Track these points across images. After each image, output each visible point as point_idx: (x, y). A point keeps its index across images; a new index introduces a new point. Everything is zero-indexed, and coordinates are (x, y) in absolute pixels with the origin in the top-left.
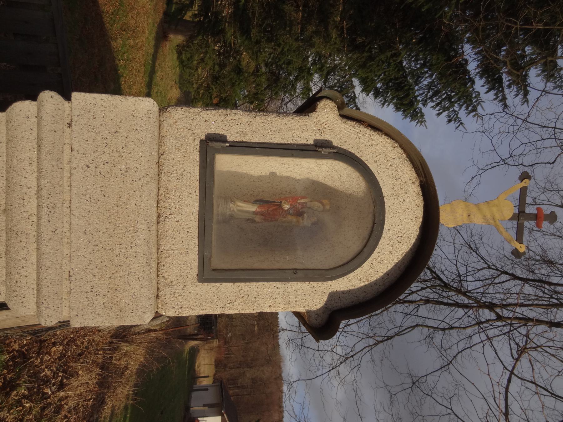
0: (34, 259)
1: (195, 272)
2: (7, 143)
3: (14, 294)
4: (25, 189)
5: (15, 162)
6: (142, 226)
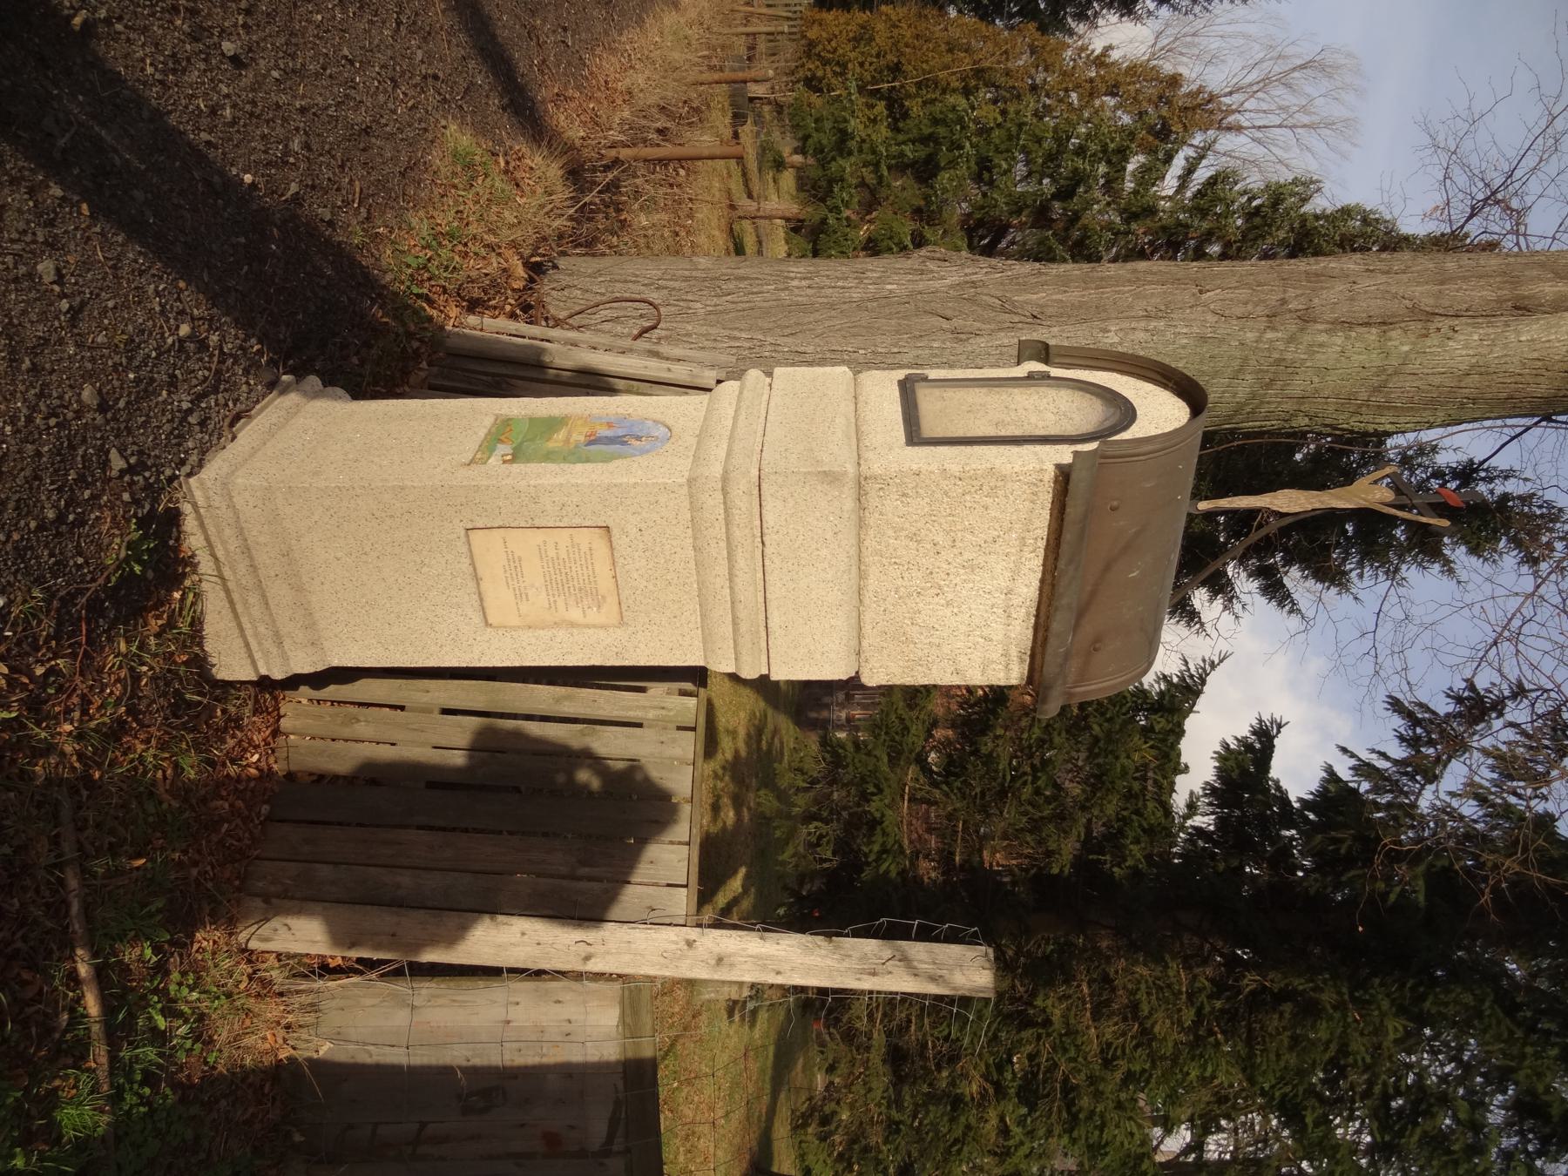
0: (725, 446)
1: (903, 439)
6: (840, 421)
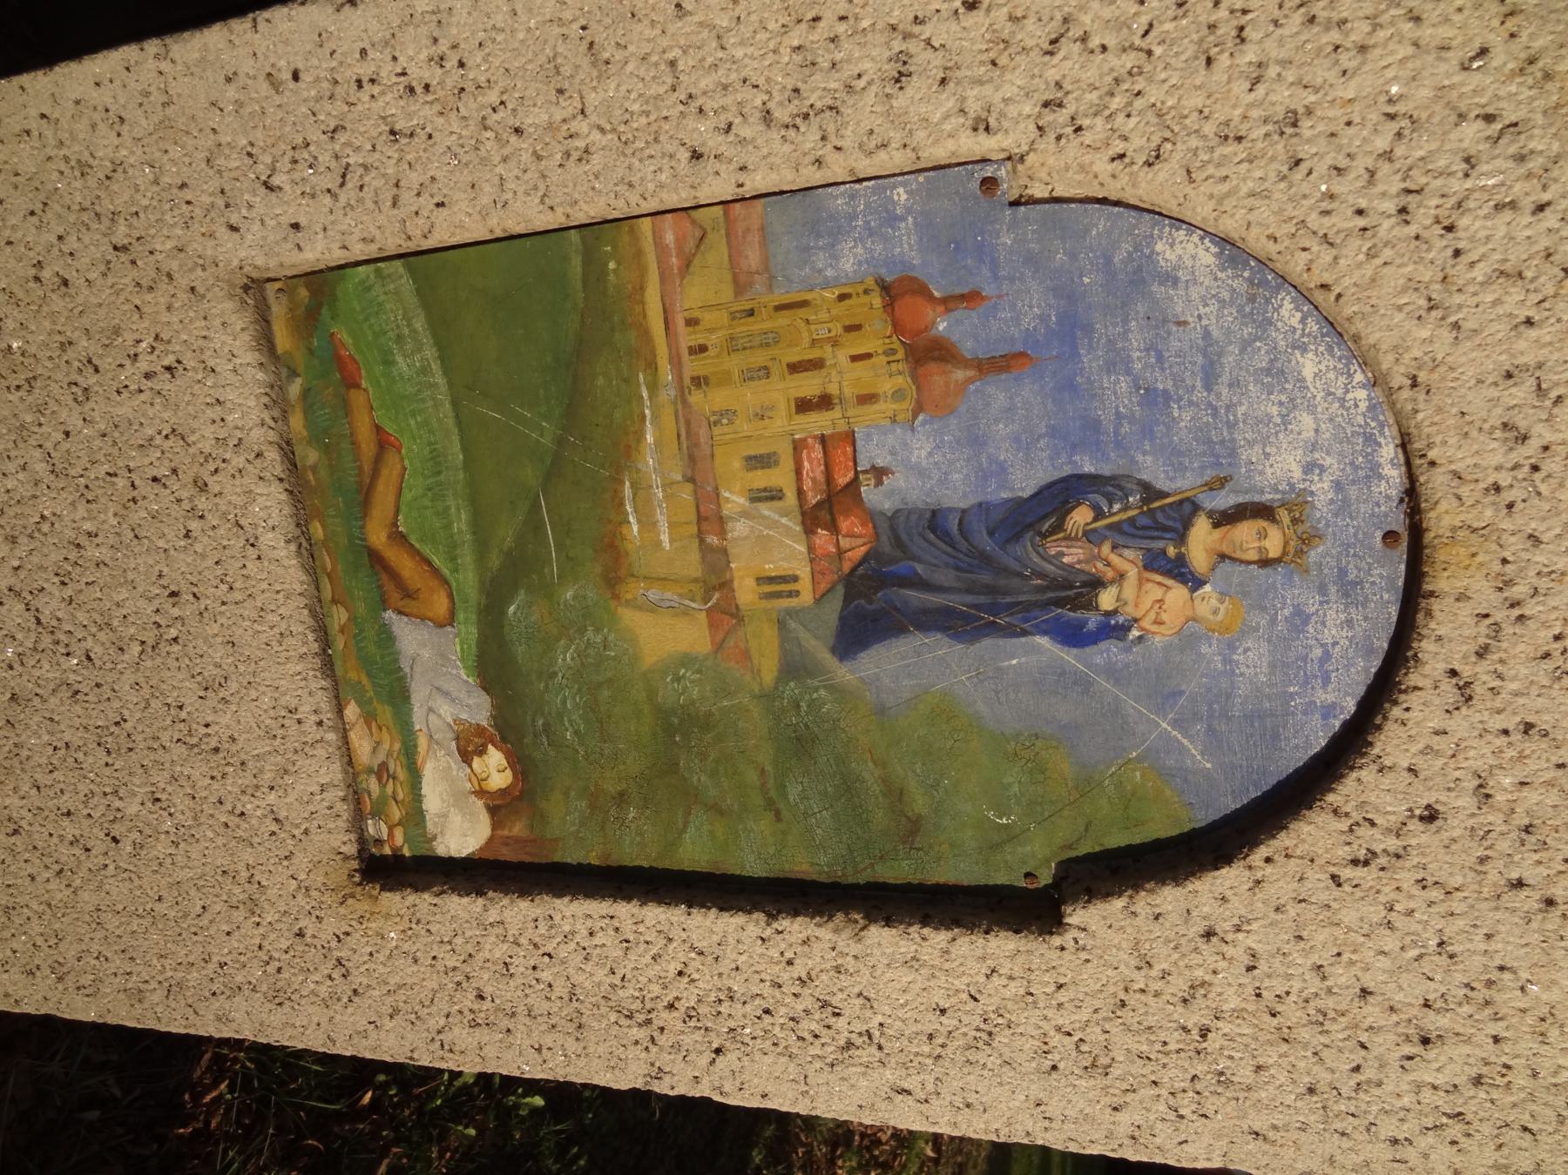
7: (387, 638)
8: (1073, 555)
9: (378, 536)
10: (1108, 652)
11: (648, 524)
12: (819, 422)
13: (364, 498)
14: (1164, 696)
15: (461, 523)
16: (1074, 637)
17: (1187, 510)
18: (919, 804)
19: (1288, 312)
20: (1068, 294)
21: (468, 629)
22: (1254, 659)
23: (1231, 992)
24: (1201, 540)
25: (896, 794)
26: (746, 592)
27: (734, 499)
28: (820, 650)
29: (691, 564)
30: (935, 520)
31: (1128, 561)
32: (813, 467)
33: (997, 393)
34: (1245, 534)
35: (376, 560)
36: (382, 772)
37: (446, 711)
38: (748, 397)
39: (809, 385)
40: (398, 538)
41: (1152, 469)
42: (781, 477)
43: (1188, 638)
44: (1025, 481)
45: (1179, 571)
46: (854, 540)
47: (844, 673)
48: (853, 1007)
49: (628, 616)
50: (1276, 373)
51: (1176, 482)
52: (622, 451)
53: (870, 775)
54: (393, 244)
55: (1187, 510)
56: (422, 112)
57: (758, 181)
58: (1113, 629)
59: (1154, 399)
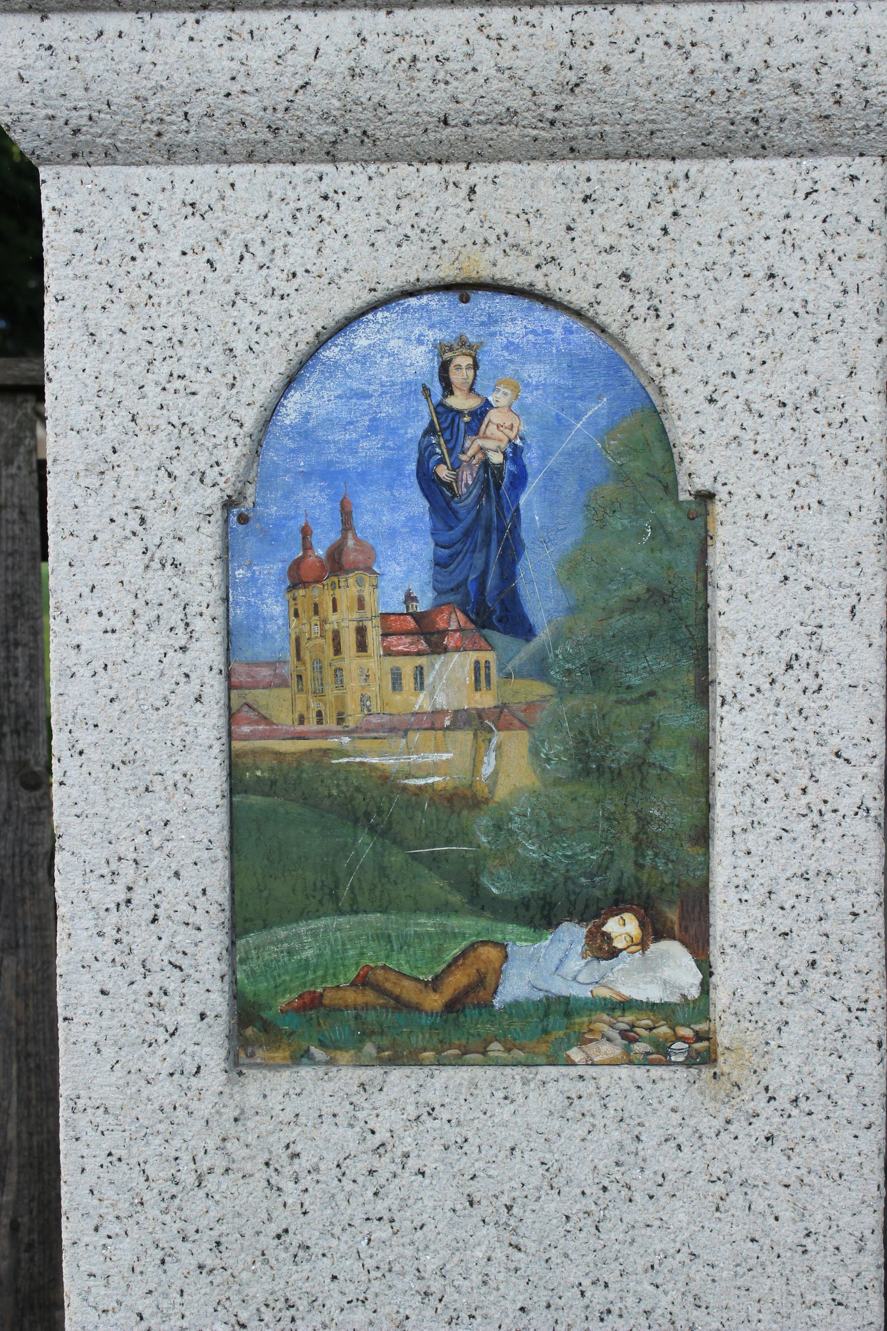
2: (171, 155)
3: (850, 96)
4: (372, 56)
5: (252, 104)
7: (515, 1008)
8: (467, 477)
9: (434, 1001)
10: (531, 458)
11: (434, 769)
12: (373, 636)
13: (400, 1004)
14: (559, 426)
15: (427, 923)
16: (520, 480)
17: (442, 410)
18: (639, 588)
19: (331, 353)
20: (307, 476)
21: (510, 932)
22: (535, 372)
23: (753, 390)
24: (460, 401)
25: (632, 605)
26: (486, 700)
27: (422, 702)
28: (525, 651)
29: (465, 737)
30: (440, 564)
31: (472, 445)
32: (402, 643)
33: (363, 520)
34: (456, 377)
35: (453, 1006)
36: (629, 1036)
37: (575, 964)
38: (353, 684)
39: (349, 640)
40: (436, 984)
41: (416, 429)
42: (407, 666)
43: (524, 411)
44: (420, 505)
45: (480, 414)
46: (454, 620)
47: (544, 635)
48: (791, 646)
49: (501, 793)
50: (364, 360)
51: (424, 415)
52: (385, 778)
53: (619, 622)
54: (221, 938)
55: (442, 410)
56: (138, 897)
57: (217, 658)
58: (515, 453)
59: (374, 427)
